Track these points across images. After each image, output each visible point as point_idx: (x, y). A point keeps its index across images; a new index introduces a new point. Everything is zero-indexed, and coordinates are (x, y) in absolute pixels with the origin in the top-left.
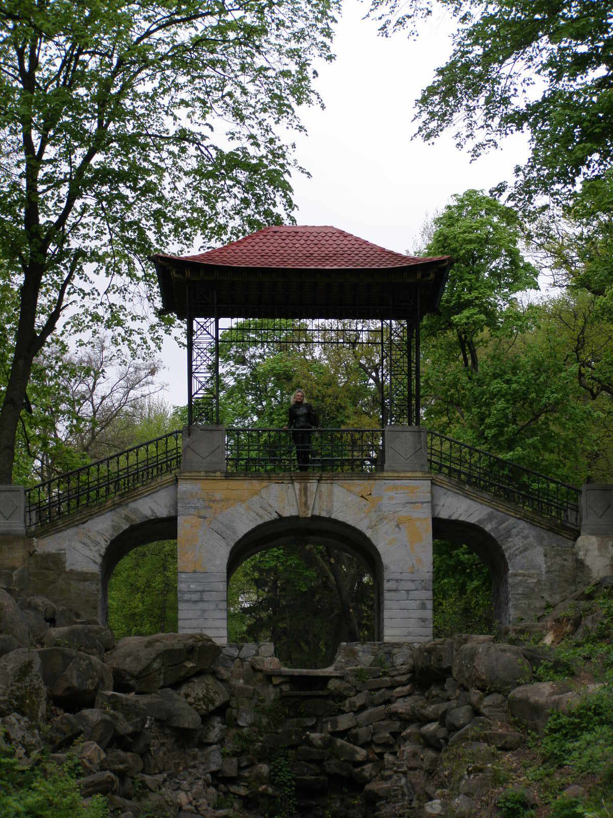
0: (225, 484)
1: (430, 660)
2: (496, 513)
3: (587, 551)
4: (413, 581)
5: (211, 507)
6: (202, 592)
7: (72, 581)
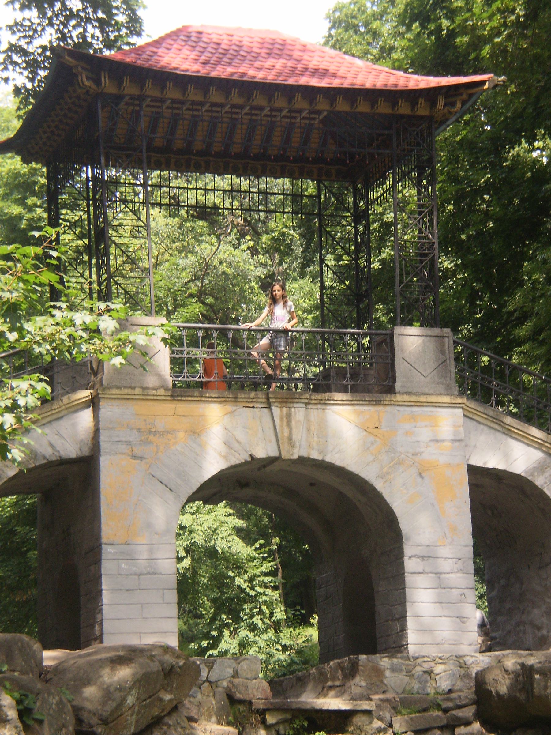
0: (170, 407)
5: (150, 442)
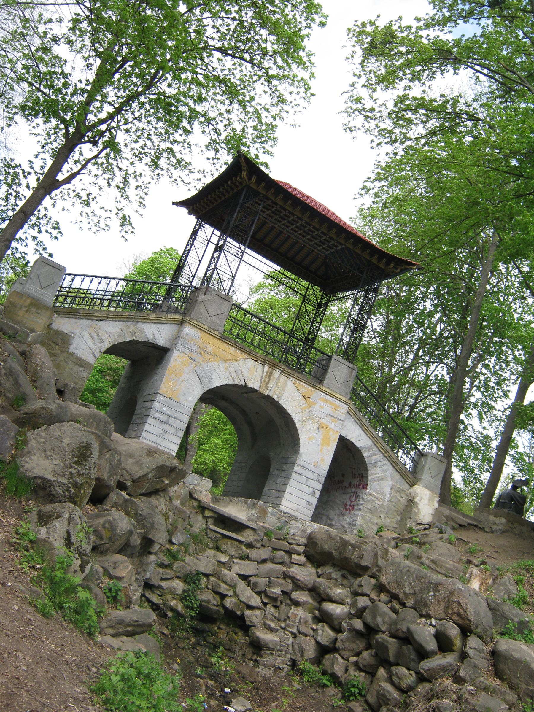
0: (217, 342)
1: (352, 555)
2: (374, 447)
3: (422, 498)
4: (314, 472)
6: (170, 416)
7: (70, 362)
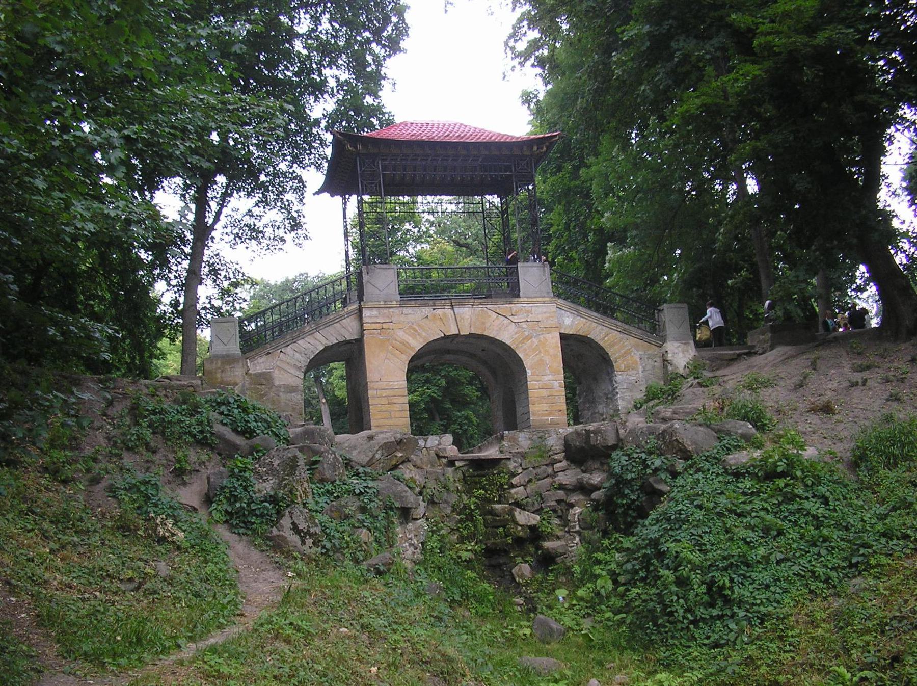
1: (597, 440)
